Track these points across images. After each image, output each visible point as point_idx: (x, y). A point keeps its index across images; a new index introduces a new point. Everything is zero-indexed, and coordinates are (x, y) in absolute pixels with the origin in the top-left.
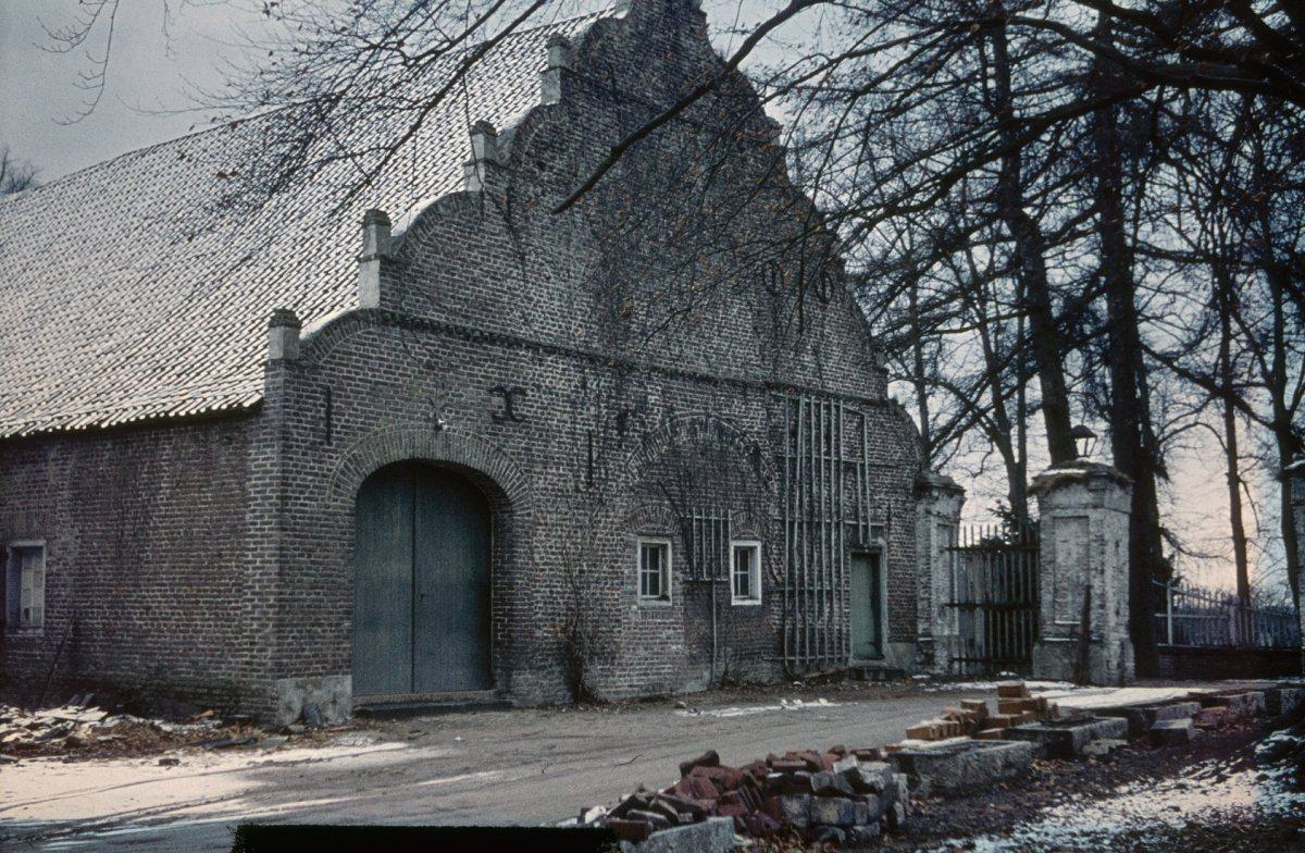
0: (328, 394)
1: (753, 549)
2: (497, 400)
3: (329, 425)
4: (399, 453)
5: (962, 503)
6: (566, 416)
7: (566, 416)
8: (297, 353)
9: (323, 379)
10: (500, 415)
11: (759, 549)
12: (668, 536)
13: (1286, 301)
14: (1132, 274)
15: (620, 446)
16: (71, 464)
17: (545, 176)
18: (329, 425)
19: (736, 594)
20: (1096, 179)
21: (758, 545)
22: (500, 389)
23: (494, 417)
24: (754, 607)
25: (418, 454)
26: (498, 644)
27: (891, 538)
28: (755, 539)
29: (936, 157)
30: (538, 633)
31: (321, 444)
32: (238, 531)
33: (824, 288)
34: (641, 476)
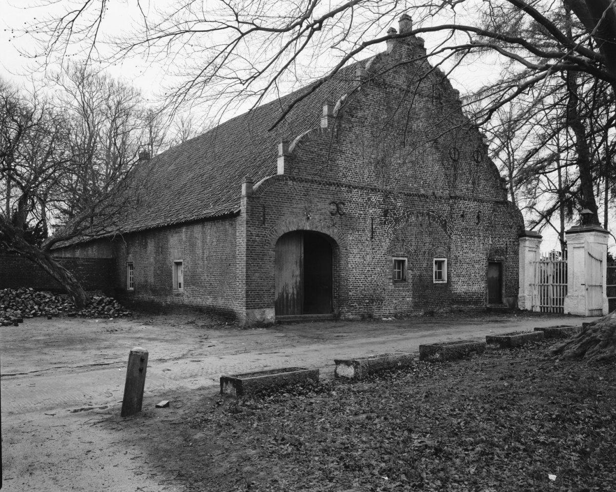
0: (264, 207)
1: (444, 261)
2: (333, 207)
3: (264, 218)
4: (293, 228)
5: (540, 242)
6: (361, 212)
7: (361, 212)
8: (253, 193)
9: (261, 201)
10: (334, 212)
11: (446, 263)
12: (406, 257)
13: (13, 186)
14: (576, 152)
15: (385, 223)
16: (189, 233)
17: (353, 120)
18: (264, 218)
19: (436, 278)
20: (582, 121)
21: (446, 260)
22: (333, 203)
23: (331, 213)
24: (443, 284)
25: (300, 228)
26: (335, 297)
27: (508, 256)
28: (444, 257)
29: (529, 160)
30: (350, 293)
31: (261, 225)
32: (234, 257)
33: (478, 158)
34: (394, 234)
